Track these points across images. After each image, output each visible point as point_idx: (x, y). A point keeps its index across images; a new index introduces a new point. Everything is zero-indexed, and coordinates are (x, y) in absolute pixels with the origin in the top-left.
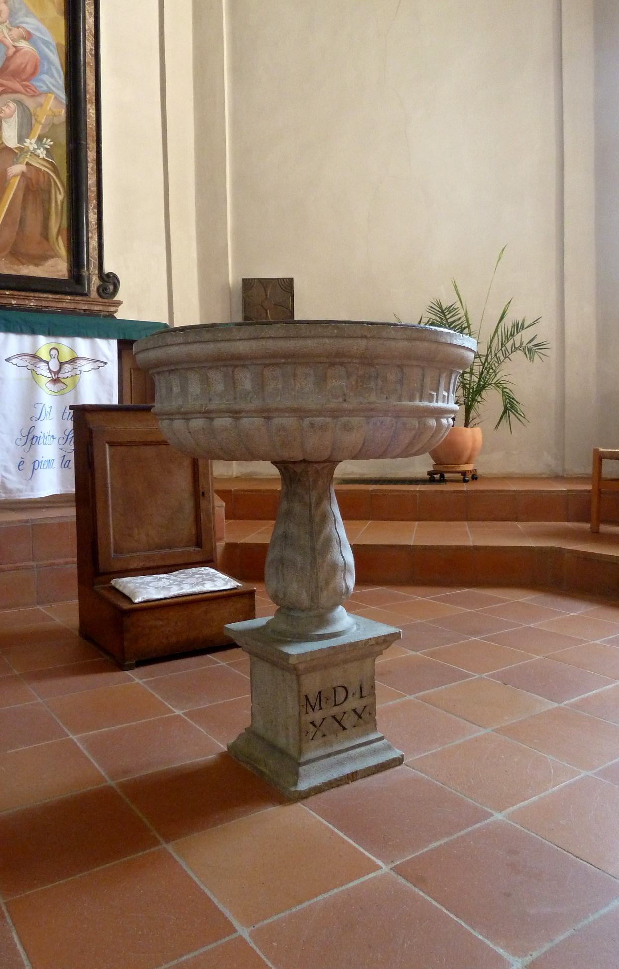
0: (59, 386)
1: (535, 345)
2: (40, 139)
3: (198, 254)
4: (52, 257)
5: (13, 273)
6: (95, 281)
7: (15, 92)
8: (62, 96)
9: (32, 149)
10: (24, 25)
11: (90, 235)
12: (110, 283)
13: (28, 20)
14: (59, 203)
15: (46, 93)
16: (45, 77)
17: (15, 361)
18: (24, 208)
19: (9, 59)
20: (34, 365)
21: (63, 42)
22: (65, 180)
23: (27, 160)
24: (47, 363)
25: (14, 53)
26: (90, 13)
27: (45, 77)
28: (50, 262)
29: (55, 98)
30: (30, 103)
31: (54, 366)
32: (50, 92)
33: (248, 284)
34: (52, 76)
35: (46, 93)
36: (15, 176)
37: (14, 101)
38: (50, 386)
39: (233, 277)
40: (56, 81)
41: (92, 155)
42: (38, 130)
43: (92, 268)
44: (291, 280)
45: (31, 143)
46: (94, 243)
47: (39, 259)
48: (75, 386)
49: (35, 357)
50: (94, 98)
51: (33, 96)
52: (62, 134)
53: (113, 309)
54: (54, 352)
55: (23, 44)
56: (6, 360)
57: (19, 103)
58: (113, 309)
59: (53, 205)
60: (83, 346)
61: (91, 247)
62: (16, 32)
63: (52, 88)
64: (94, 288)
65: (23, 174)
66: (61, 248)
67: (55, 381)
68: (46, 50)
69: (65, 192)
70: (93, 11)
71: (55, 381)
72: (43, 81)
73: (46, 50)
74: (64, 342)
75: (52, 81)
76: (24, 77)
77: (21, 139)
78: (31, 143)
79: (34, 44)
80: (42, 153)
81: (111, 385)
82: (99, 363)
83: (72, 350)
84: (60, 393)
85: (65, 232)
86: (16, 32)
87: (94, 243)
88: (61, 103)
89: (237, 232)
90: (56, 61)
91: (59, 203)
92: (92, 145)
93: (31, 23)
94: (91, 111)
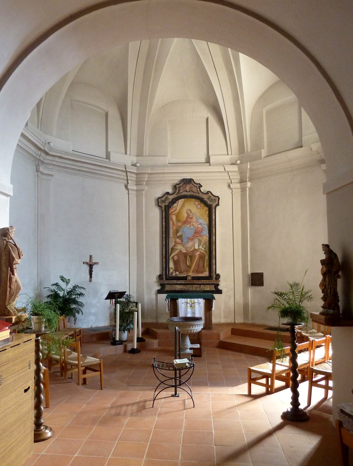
0: (192, 307)
1: (310, 298)
2: (203, 246)
3: (242, 266)
4: (205, 271)
5: (197, 276)
6: (214, 276)
7: (198, 237)
8: (208, 235)
9: (201, 248)
10: (199, 222)
11: (213, 266)
12: (218, 276)
13: (200, 220)
14: (207, 259)
15: (204, 235)
16: (204, 232)
17: (183, 303)
18: (199, 261)
19: (196, 230)
20: (187, 304)
21: (208, 223)
22: (208, 254)
23: (200, 251)
24: (189, 303)
25: (197, 228)
26: (214, 215)
27: (204, 232)
28: (205, 273)
29: (206, 236)
30: (200, 238)
31: (191, 304)
32: (205, 235)
33: (252, 274)
34: (205, 231)
35: (204, 235)
36: (197, 255)
37: (197, 239)
38: (190, 307)
39: (249, 272)
40: (206, 232)
41: (214, 247)
42: (202, 244)
43: (214, 273)
44: (262, 273)
45: (201, 247)
46: (214, 267)
47: (202, 272)
48: (194, 308)
49: (187, 303)
50: (215, 234)
51: (201, 237)
52: (207, 244)
53: (218, 282)
54: (191, 301)
55: (199, 226)
56: (182, 303)
57: (198, 239)
58: (218, 282)
59: (205, 260)
60: (196, 300)
61: (214, 268)
62: (198, 223)
63: (205, 234)
64: (214, 278)
65: (199, 254)
66: (207, 270)
67: (191, 307)
68: (205, 226)
69: (208, 256)
70: (214, 215)
71: (191, 307)
72: (204, 233)
73: (205, 226)
74: (192, 299)
75: (205, 232)
76: (199, 233)
77: (199, 247)
78: (201, 247)
79: (202, 225)
80: (203, 249)
81: (201, 307)
82: (199, 303)
83: (194, 301)
84: (192, 309)
85: (208, 266)
86: (198, 223)
87: (214, 267)
88: (207, 237)
89: (251, 261)
90: (206, 228)
91: (207, 259)
92: (214, 245)
93: (201, 221)
94: (214, 237)
